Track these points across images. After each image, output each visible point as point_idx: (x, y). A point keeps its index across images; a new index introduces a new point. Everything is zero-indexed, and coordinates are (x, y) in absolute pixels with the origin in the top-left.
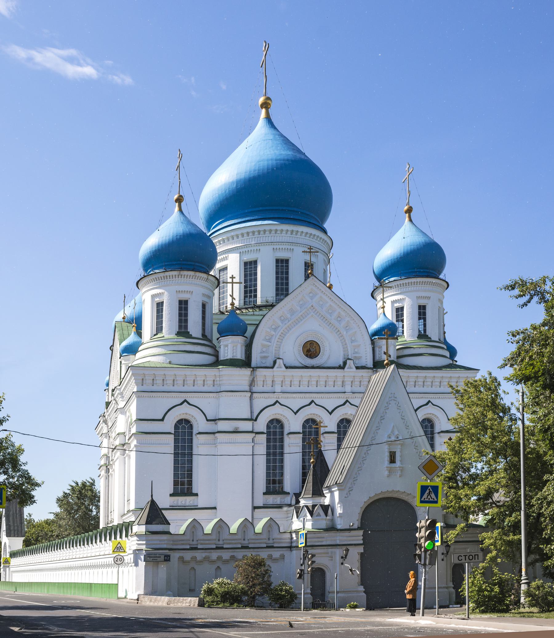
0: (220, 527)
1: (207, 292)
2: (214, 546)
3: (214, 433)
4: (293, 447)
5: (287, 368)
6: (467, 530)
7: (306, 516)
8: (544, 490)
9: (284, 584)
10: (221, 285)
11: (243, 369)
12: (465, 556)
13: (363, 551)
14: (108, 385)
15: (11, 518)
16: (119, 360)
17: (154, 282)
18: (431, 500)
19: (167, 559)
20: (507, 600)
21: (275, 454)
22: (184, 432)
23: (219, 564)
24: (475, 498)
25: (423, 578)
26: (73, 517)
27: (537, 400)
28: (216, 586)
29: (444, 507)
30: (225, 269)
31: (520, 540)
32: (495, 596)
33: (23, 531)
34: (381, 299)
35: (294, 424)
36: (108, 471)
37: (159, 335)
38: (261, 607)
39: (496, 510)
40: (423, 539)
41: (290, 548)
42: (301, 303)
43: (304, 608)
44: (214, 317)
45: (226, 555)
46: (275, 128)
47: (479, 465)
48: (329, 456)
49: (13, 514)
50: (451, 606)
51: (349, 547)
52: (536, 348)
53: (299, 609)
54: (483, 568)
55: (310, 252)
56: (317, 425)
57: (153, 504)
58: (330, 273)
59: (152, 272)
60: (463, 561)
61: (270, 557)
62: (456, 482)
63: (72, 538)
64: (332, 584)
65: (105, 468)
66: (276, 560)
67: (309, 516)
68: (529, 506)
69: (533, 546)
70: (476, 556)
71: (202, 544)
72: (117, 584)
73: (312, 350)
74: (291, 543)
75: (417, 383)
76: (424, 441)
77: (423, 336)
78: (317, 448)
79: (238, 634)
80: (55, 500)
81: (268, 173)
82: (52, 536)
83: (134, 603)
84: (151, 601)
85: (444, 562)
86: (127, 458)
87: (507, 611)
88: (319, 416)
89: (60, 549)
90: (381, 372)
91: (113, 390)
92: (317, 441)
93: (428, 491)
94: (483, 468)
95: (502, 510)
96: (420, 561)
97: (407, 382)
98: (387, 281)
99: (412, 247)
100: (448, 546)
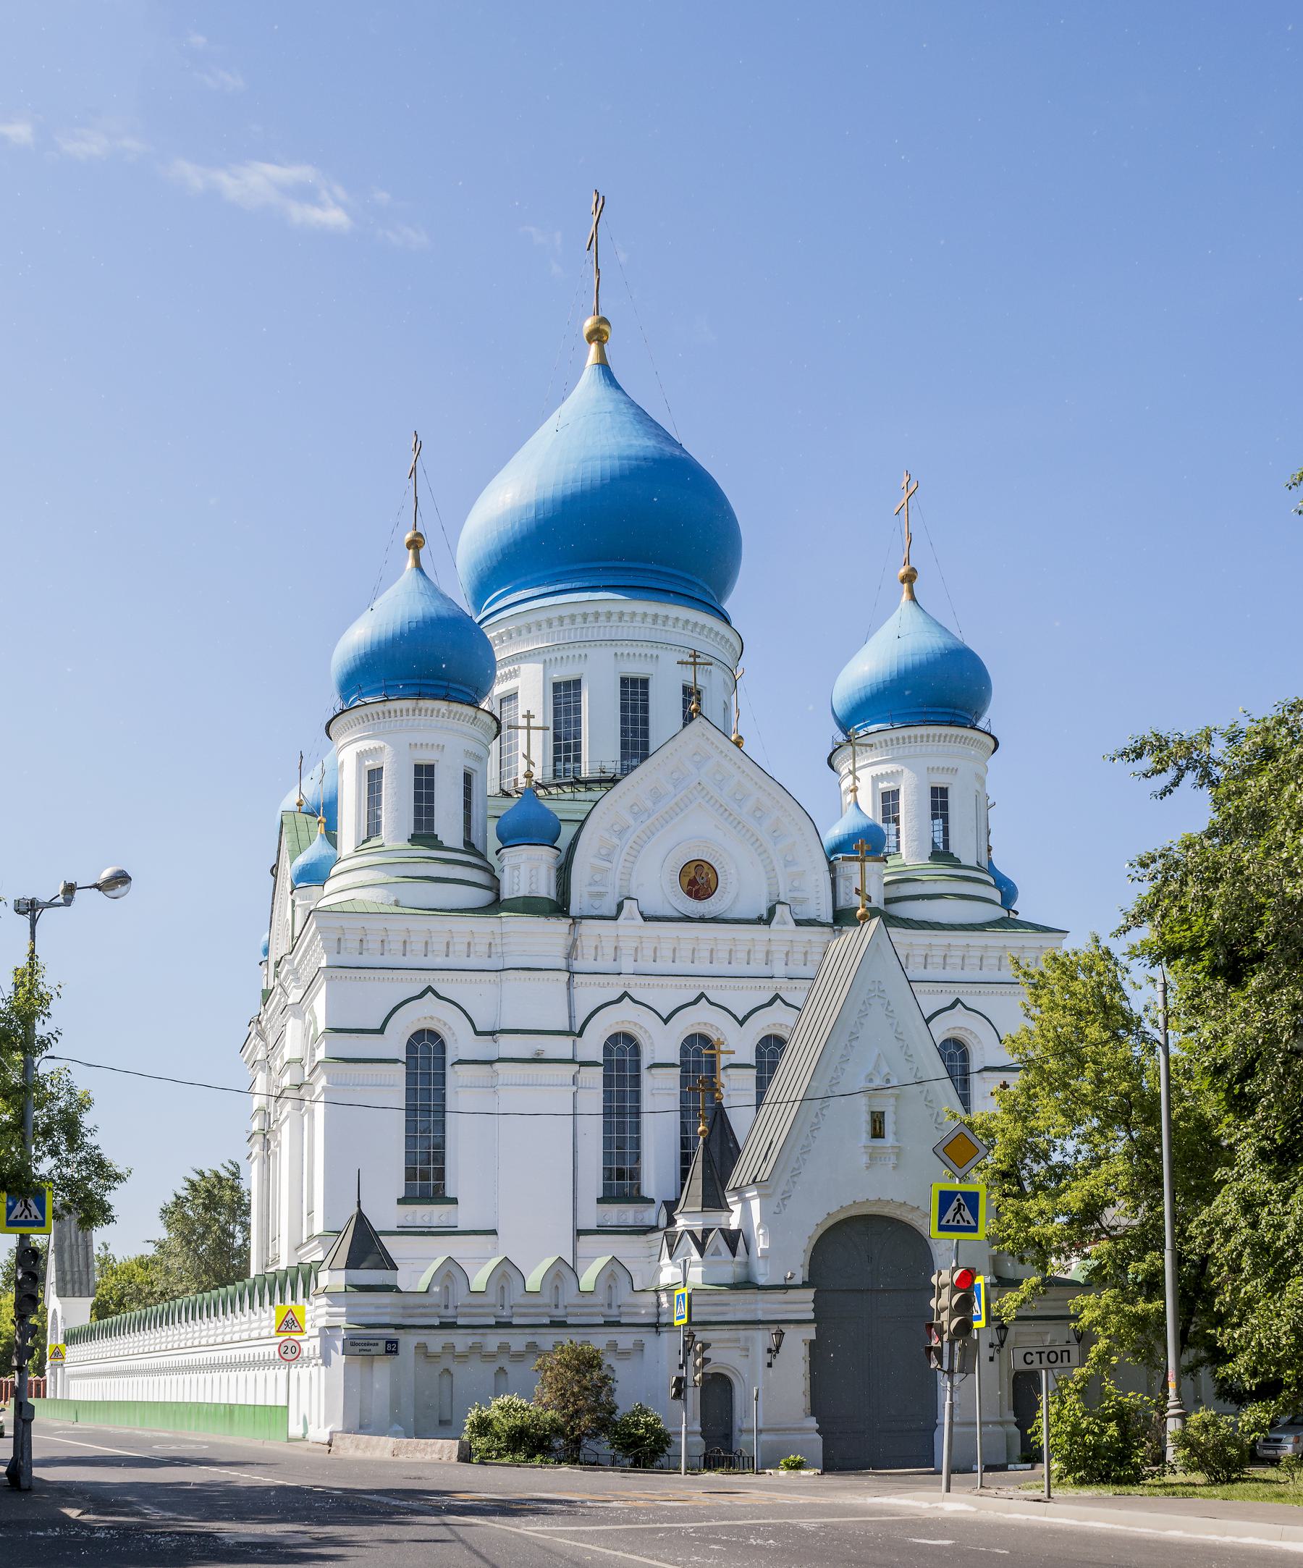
0: (505, 1275)
1: (478, 750)
2: (492, 1321)
3: (490, 1062)
4: (660, 1096)
5: (645, 919)
6: (1045, 1292)
7: (689, 1253)
8: (1214, 1204)
9: (644, 1412)
10: (504, 732)
11: (553, 920)
12: (1040, 1353)
13: (814, 1337)
14: (266, 951)
15: (66, 1256)
16: (290, 897)
17: (362, 725)
18: (962, 1223)
19: (392, 1348)
20: (1137, 1456)
21: (621, 1113)
22: (426, 1058)
23: (504, 1362)
24: (1063, 1219)
25: (948, 1402)
26: (195, 1251)
27: (1197, 1001)
28: (497, 1413)
29: (992, 1239)
30: (511, 697)
31: (1162, 1314)
32: (1109, 1447)
33: (91, 1285)
34: (850, 772)
35: (661, 1044)
36: (266, 1144)
37: (374, 842)
38: (594, 1464)
39: (1105, 1245)
40: (947, 1312)
41: (656, 1326)
42: (675, 776)
43: (687, 1468)
44: (491, 802)
45: (518, 1341)
46: (618, 387)
47: (1070, 1146)
48: (740, 1120)
49: (71, 1246)
50: (1010, 1466)
51: (784, 1328)
52: (1193, 889)
53: (677, 1469)
54: (1082, 1378)
55: (694, 664)
56: (712, 1048)
57: (361, 1219)
58: (738, 711)
59: (358, 703)
60: (1036, 1365)
61: (613, 1346)
62: (1020, 1184)
63: (193, 1298)
64: (747, 1413)
65: (259, 1138)
66: (625, 1354)
67: (696, 1256)
68: (1182, 1236)
69: (1192, 1328)
70: (1065, 1354)
71: (465, 1315)
72: (287, 1407)
73: (700, 881)
74: (659, 1315)
75: (929, 960)
76: (946, 1091)
77: (942, 854)
78: (713, 1099)
79: (543, 1532)
80: (157, 1213)
81: (603, 486)
82: (151, 1294)
83: (322, 1451)
84: (357, 1447)
85: (995, 1365)
86: (306, 1118)
87: (1135, 1480)
88: (717, 1029)
89: (167, 1324)
90: (851, 933)
91: (278, 964)
92: (713, 1084)
93: (955, 1204)
94: (1079, 1152)
95: (1121, 1246)
96: (941, 1362)
97: (907, 957)
98: (862, 733)
99: (917, 658)
100: (1003, 1327)
